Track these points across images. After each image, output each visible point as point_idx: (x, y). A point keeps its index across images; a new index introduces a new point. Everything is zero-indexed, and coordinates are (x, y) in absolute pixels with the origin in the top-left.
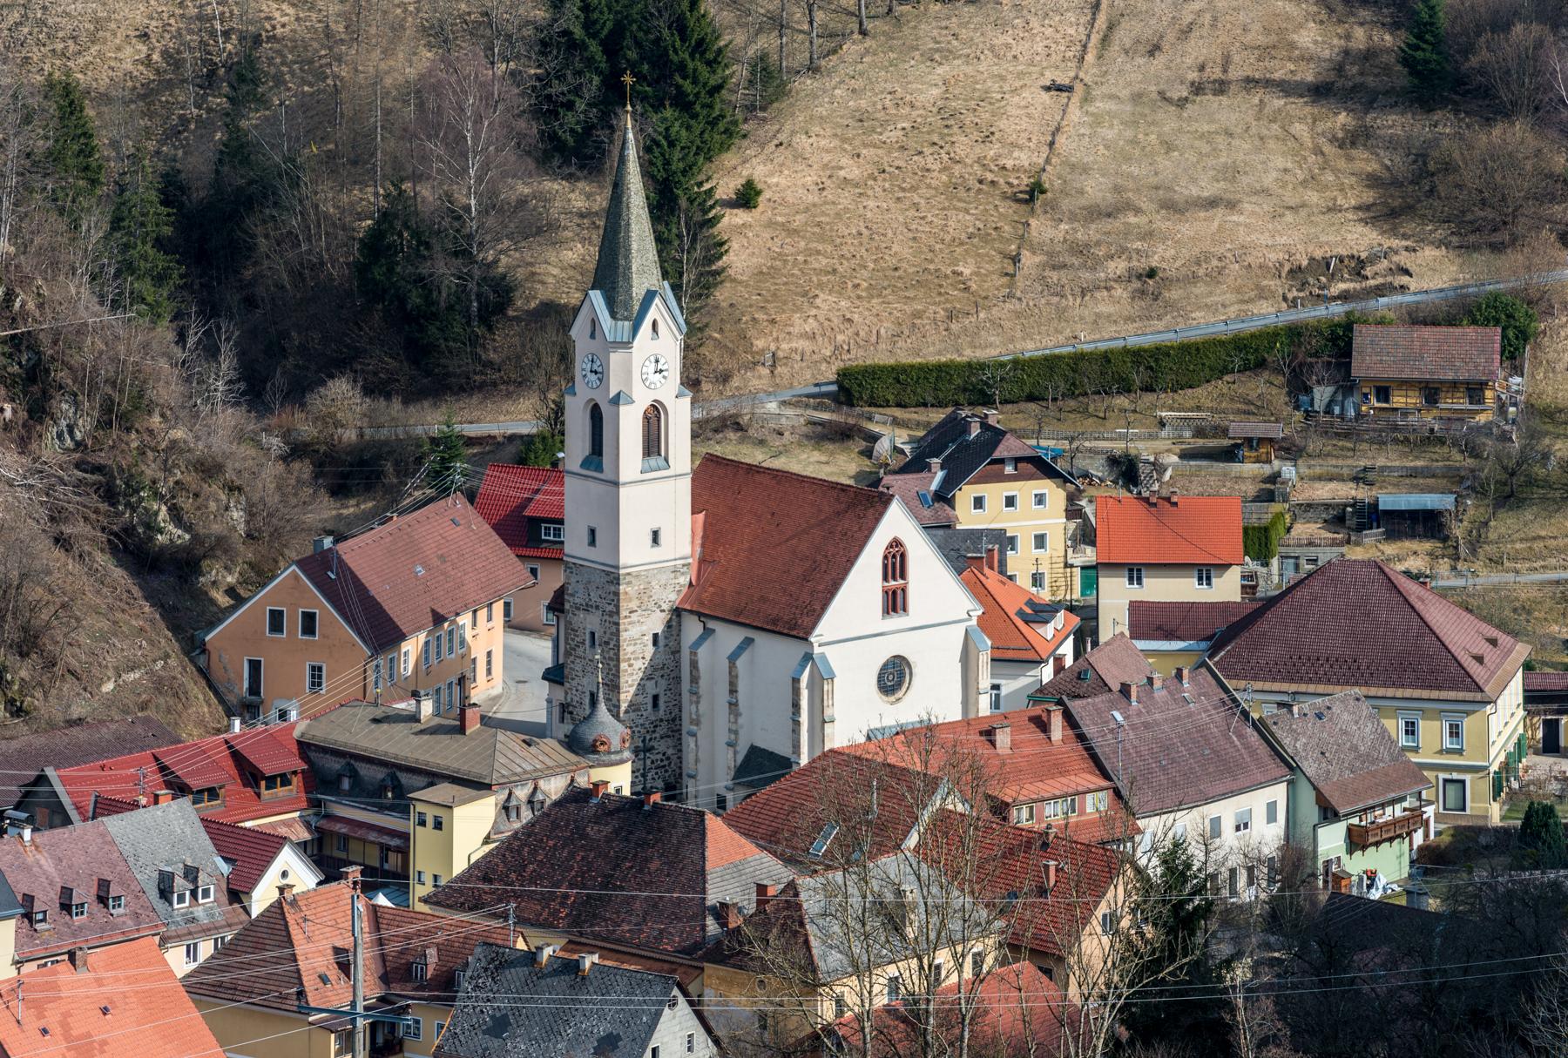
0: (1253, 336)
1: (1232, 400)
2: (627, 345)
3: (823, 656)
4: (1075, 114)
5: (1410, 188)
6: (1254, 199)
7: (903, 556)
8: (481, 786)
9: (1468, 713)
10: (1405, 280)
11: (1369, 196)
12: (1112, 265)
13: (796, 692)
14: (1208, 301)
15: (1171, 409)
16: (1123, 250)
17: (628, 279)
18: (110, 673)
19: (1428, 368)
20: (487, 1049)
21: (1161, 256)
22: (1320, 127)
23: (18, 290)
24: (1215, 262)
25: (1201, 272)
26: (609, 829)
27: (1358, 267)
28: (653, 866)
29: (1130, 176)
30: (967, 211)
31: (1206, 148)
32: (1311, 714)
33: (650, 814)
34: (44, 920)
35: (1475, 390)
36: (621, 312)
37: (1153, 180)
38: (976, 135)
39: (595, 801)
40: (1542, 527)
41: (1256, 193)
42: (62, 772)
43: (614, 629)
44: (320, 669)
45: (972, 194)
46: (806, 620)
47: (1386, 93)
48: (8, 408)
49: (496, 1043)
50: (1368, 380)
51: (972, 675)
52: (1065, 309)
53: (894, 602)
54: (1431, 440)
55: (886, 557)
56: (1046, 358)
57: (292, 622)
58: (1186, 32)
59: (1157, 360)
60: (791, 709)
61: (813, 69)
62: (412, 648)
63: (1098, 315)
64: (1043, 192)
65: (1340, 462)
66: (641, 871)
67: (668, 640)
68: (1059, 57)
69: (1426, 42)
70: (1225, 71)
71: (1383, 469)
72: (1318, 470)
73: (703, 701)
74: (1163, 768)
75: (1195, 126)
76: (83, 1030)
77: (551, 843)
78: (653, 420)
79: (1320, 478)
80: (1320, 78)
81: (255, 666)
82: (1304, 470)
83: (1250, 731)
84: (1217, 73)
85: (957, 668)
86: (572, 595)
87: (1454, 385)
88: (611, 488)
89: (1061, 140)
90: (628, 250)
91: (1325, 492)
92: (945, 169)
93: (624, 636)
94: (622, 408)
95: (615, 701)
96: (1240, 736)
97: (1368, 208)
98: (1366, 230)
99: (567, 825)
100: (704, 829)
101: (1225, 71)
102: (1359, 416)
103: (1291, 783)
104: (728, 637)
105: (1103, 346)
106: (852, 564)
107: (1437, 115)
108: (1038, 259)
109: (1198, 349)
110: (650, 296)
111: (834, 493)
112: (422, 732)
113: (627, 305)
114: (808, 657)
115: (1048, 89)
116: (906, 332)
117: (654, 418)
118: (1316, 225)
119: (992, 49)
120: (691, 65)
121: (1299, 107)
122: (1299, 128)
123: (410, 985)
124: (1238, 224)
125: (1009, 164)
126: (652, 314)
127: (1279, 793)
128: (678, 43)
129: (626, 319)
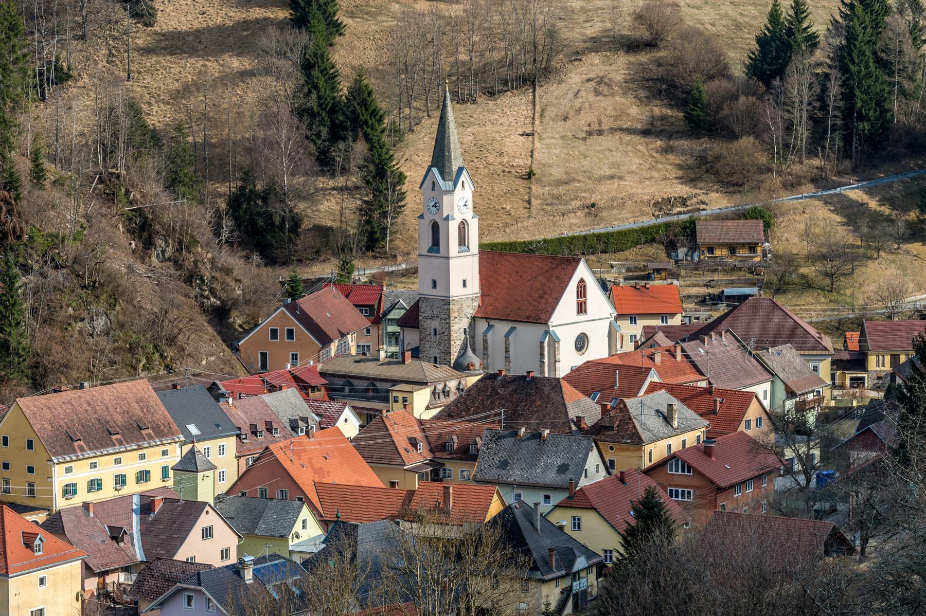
0: (649, 227)
1: (641, 255)
2: (451, 192)
3: (553, 331)
4: (537, 144)
5: (697, 170)
6: (630, 175)
7: (585, 287)
8: (423, 384)
9: (822, 361)
10: (704, 206)
11: (680, 173)
12: (573, 203)
13: (542, 348)
14: (620, 216)
15: (615, 260)
16: (576, 198)
17: (450, 162)
18: (204, 356)
19: (731, 238)
20: (500, 475)
21: (595, 198)
22: (650, 147)
23: (131, 190)
24: (620, 201)
25: (615, 205)
26: (510, 389)
27: (684, 202)
28: (538, 403)
29: (571, 167)
30: (501, 184)
31: (602, 156)
32: (775, 353)
33: (529, 382)
34: (246, 438)
35: (752, 248)
36: (447, 177)
37: (583, 169)
38: (495, 154)
39: (499, 378)
40: (798, 301)
41: (630, 173)
42: (224, 382)
43: (447, 326)
44: (296, 355)
45: (501, 177)
46: (545, 316)
47: (676, 133)
48: (133, 243)
49: (504, 472)
50: (703, 244)
51: (613, 344)
52: (556, 221)
53: (581, 308)
54: (735, 269)
55: (578, 287)
56: (558, 239)
58: (579, 111)
59: (607, 239)
60: (539, 356)
61: (411, 130)
62: (333, 347)
63: (571, 224)
64: (534, 175)
65: (697, 279)
66: (531, 406)
68: (523, 123)
69: (698, 107)
70: (600, 126)
71: (718, 281)
72: (688, 283)
73: (490, 358)
74: (724, 373)
75: (594, 148)
76: (319, 466)
77: (481, 398)
78: (462, 229)
79: (689, 286)
80: (644, 128)
81: (264, 355)
82: (682, 283)
83: (752, 359)
84: (597, 127)
85: (607, 339)
86: (423, 313)
87: (743, 245)
88: (445, 260)
89: (535, 154)
90: (449, 148)
91: (694, 291)
92: (485, 167)
93: (452, 329)
94: (450, 222)
95: (448, 359)
96: (750, 361)
97: (681, 178)
98: (683, 186)
99: (487, 390)
100: (561, 386)
101: (600, 126)
102: (700, 260)
103: (772, 382)
104: (502, 328)
105: (583, 234)
106: (565, 290)
107: (703, 140)
108: (539, 202)
109: (626, 234)
110: (460, 170)
111: (549, 260)
112: (382, 364)
113: (450, 174)
114: (547, 332)
115: (522, 135)
116: (486, 233)
117: (463, 226)
118: (660, 185)
119: (490, 121)
120: (370, 122)
121: (637, 139)
122: (640, 147)
123: (445, 453)
124: (626, 185)
125: (515, 164)
126: (462, 178)
127: (767, 386)
128: (364, 112)
129: (450, 180)
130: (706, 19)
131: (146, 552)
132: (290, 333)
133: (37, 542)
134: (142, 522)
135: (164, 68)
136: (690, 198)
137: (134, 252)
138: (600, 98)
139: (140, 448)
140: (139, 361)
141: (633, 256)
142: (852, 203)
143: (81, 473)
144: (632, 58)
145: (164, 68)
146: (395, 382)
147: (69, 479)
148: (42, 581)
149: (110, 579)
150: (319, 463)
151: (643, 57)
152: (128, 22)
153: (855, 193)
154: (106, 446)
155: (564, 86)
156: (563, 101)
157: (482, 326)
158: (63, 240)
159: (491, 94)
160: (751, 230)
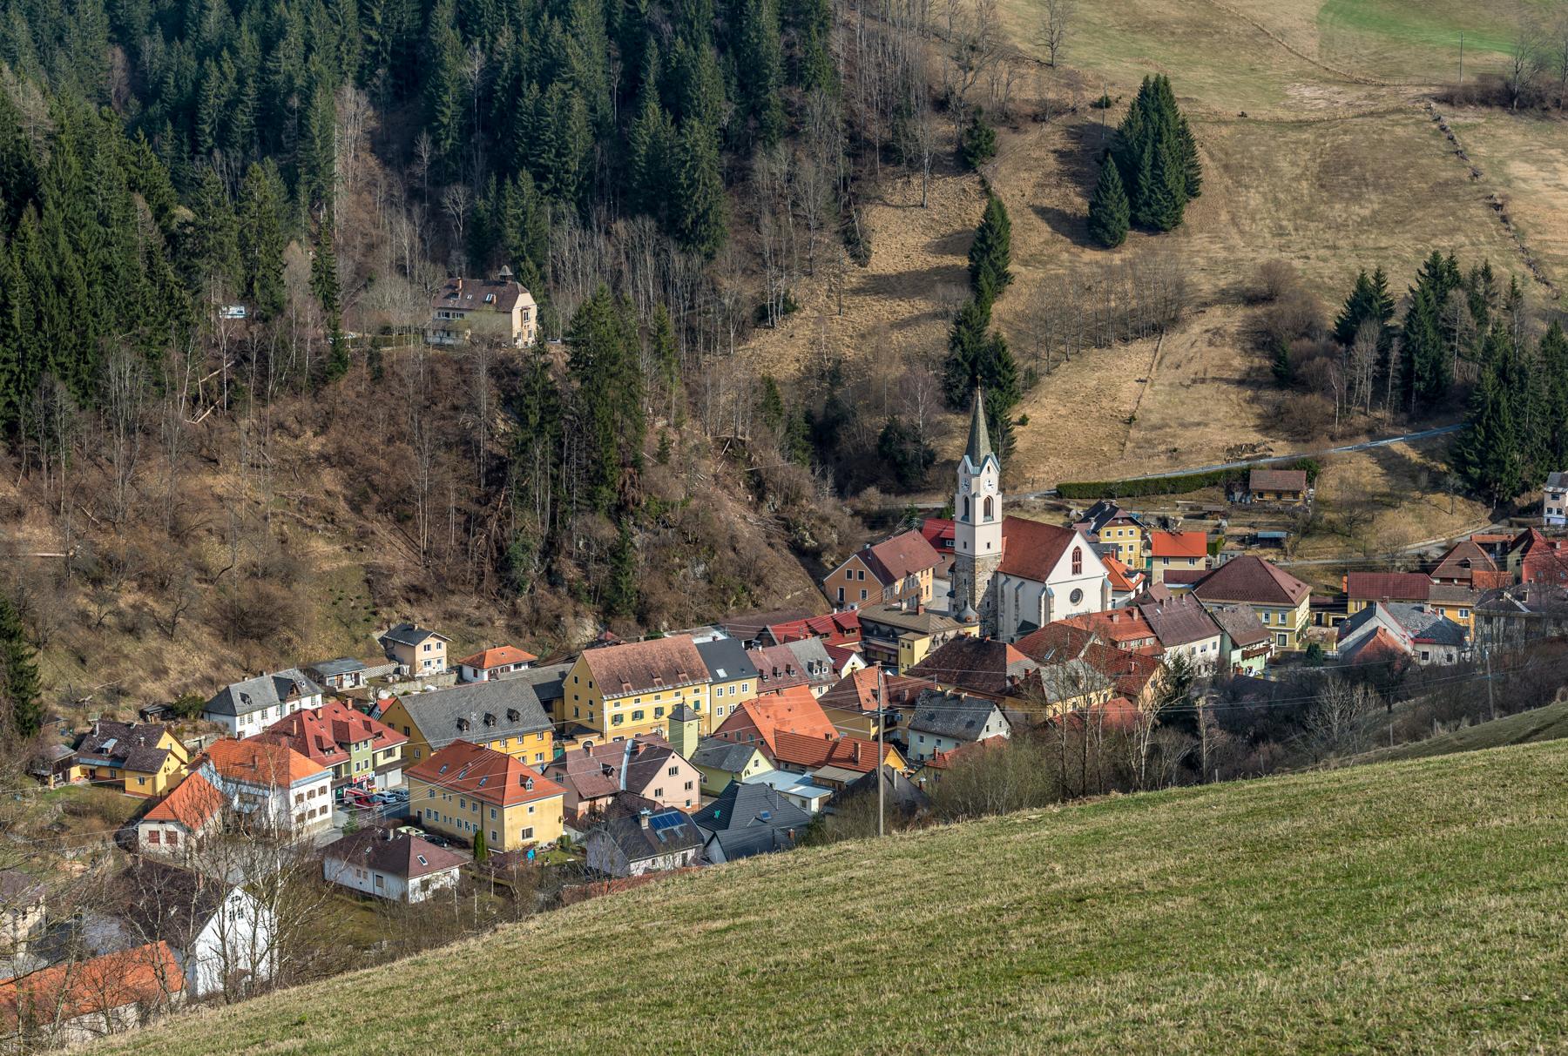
4: (1147, 391)
8: (924, 634)
11: (1258, 422)
21: (1178, 444)
27: (1253, 448)
35: (1296, 494)
53: (1077, 569)
57: (856, 575)
61: (1049, 373)
62: (899, 585)
67: (993, 583)
81: (842, 590)
87: (1288, 492)
89: (1142, 400)
91: (1237, 531)
104: (1015, 582)
114: (1045, 589)
117: (988, 502)
121: (1232, 388)
122: (1233, 396)
127: (1217, 639)
130: (1327, 272)
131: (628, 783)
132: (861, 573)
133: (529, 782)
134: (630, 760)
135: (868, 305)
136: (1259, 445)
137: (750, 504)
138: (1212, 348)
139: (675, 688)
140: (729, 599)
141: (1194, 497)
142: (1394, 455)
143: (627, 707)
144: (1249, 311)
145: (868, 305)
146: (907, 630)
147: (617, 711)
148: (531, 810)
149: (598, 802)
150: (783, 714)
151: (1259, 311)
152: (848, 261)
153: (1397, 446)
154: (647, 686)
155: (1185, 336)
156: (1180, 350)
157: (1002, 578)
158: (673, 507)
159: (1125, 340)
160: (1296, 478)
